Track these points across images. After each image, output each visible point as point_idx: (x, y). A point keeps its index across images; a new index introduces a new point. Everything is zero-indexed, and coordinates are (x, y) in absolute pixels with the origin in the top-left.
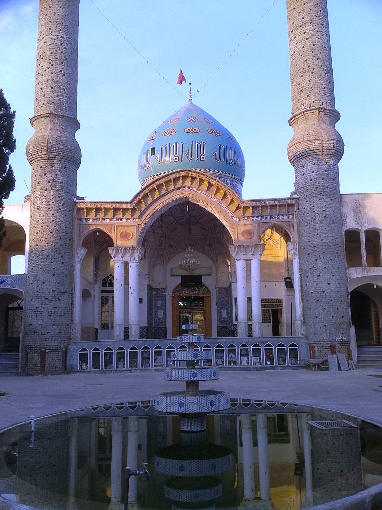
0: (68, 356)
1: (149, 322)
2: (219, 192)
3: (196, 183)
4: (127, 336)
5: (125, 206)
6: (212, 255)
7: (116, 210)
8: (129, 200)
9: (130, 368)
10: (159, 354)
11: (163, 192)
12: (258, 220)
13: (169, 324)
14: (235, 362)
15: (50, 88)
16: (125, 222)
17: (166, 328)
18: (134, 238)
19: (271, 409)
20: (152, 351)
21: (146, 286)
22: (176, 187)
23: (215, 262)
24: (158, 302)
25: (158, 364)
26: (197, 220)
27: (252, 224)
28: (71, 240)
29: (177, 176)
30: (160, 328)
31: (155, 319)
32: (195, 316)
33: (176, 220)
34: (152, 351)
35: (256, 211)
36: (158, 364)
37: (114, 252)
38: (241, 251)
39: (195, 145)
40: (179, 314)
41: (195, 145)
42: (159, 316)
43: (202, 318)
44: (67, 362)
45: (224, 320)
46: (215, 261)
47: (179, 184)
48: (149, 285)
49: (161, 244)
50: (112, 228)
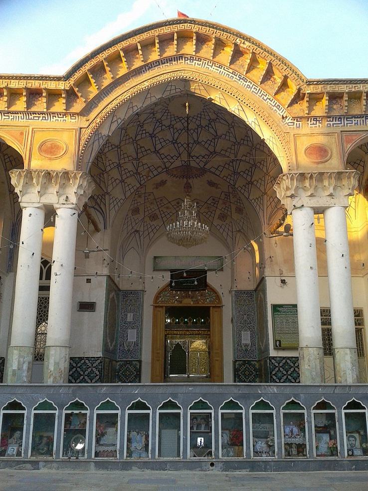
1: (106, 349)
2: (254, 68)
3: (207, 50)
5: (52, 85)
6: (225, 234)
7: (33, 94)
8: (62, 72)
9: (34, 458)
10: (108, 421)
11: (138, 63)
12: (339, 126)
13: (146, 356)
14: (301, 448)
16: (53, 122)
17: (140, 362)
18: (68, 155)
19: (204, 396)
20: (92, 414)
21: (104, 280)
22: (165, 55)
23: (230, 248)
24: (129, 315)
25: (106, 448)
26: (202, 165)
27: (328, 134)
30: (130, 362)
31: (122, 345)
32: (192, 342)
33: (164, 163)
34: (92, 414)
35: (335, 107)
36: (106, 448)
37: (21, 184)
38: (305, 189)
40: (166, 340)
42: (129, 340)
43: (204, 347)
45: (246, 350)
46: (231, 247)
47: (171, 51)
48: (110, 279)
49: (136, 211)
50: (22, 134)
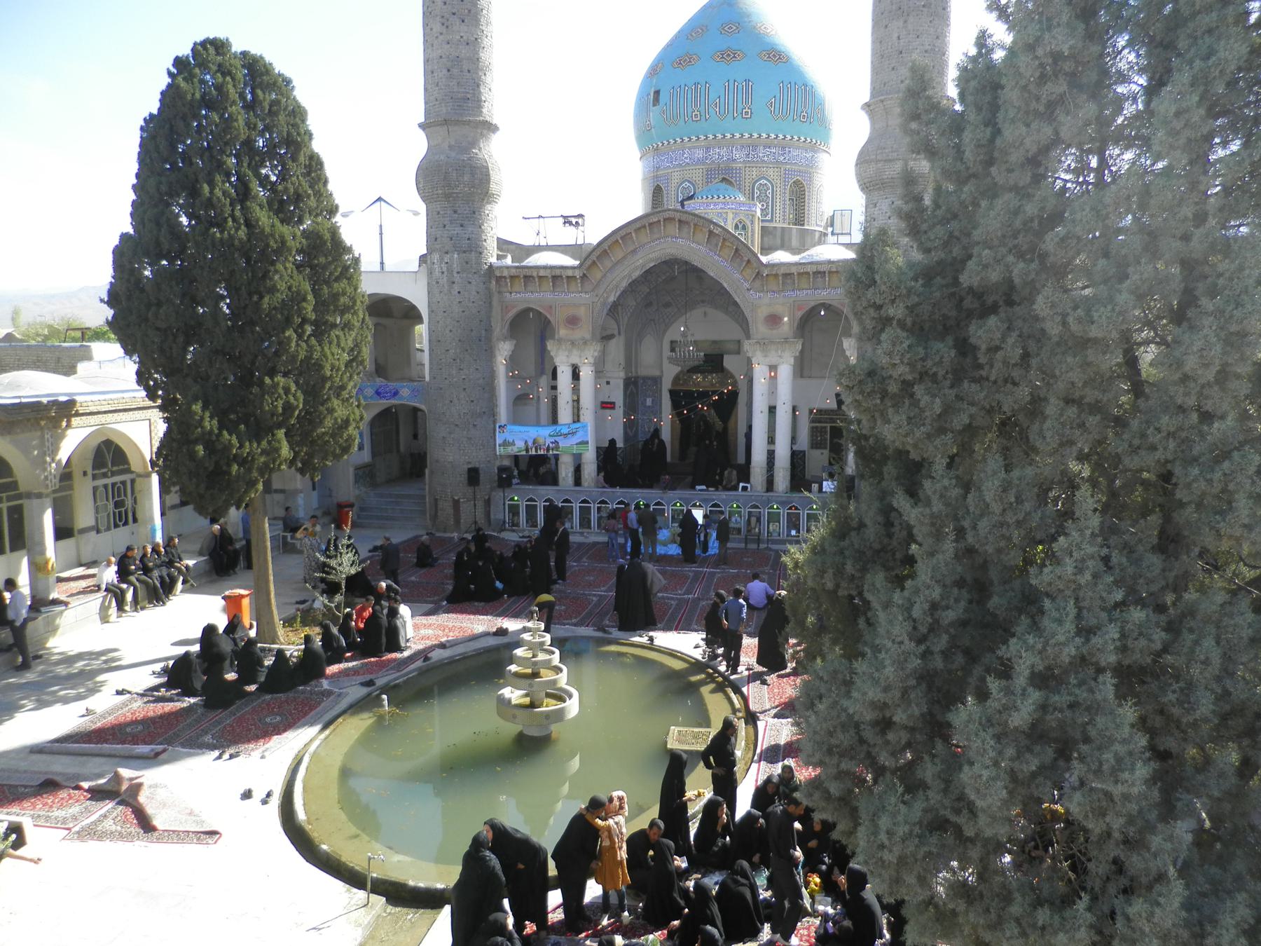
0: (492, 507)
4: (578, 481)
15: (445, 71)
28: (489, 330)
29: (656, 220)
39: (731, 87)
41: (731, 87)
44: (492, 517)
50: (551, 307)
